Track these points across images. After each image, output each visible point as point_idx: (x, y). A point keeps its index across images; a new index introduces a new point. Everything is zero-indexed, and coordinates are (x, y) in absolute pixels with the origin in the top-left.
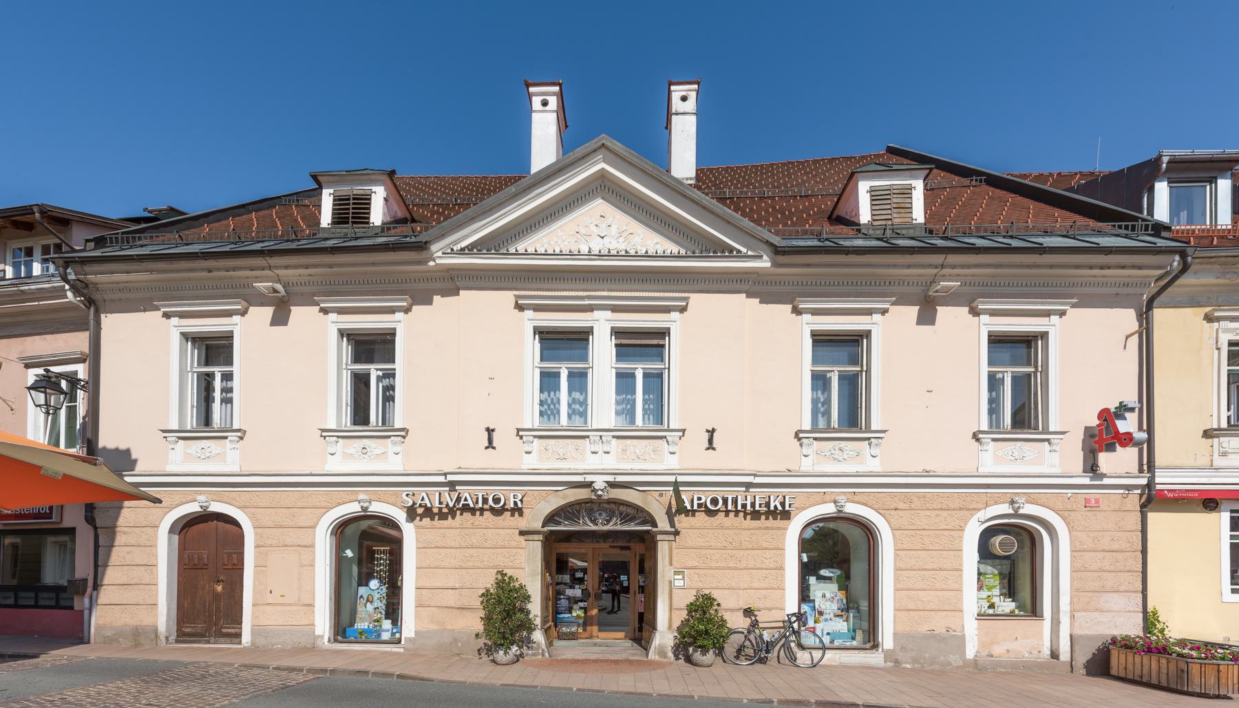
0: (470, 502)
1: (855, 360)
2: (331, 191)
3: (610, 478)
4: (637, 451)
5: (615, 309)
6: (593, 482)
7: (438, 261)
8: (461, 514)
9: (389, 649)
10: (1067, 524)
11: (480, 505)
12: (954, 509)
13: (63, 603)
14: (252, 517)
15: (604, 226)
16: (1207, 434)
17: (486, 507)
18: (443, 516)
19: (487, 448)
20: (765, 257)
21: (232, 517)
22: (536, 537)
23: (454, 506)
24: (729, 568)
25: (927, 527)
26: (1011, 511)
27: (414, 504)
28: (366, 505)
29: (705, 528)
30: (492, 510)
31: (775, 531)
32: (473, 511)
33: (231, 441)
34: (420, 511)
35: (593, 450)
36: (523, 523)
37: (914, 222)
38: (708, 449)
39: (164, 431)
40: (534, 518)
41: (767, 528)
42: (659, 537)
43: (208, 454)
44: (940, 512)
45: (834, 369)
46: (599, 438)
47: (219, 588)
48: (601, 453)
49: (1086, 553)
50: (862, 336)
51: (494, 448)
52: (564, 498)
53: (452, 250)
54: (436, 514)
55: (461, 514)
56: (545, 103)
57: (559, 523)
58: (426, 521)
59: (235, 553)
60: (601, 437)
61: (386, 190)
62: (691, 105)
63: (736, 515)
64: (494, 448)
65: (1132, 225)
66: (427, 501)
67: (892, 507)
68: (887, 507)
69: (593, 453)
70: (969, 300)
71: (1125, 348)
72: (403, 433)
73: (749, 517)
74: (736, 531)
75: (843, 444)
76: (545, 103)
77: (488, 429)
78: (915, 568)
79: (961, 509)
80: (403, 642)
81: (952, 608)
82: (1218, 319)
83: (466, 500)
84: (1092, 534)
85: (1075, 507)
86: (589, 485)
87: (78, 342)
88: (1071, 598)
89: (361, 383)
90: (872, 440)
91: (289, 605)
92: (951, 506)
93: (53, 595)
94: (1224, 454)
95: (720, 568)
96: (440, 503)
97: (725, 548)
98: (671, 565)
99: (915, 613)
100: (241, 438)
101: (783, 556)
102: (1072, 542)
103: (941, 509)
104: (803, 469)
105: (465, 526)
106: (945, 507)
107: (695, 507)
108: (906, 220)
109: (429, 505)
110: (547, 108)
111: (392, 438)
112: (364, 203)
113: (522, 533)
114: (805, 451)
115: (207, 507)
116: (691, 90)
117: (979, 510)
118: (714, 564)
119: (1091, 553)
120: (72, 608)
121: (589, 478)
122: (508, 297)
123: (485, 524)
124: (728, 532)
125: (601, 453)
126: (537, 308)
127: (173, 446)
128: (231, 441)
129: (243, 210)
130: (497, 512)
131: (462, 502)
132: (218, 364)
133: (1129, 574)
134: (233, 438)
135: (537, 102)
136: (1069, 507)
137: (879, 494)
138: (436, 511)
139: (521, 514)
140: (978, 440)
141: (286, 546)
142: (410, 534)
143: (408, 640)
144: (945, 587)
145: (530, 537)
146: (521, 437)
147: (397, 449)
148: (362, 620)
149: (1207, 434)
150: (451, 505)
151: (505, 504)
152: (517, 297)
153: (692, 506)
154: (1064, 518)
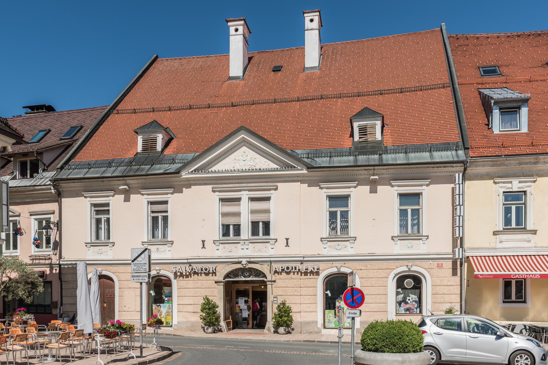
0: (196, 270)
2: (142, 136)
3: (248, 260)
4: (259, 248)
5: (249, 190)
6: (241, 261)
7: (184, 177)
8: (194, 275)
9: (168, 329)
10: (430, 274)
11: (200, 271)
12: (384, 269)
13: (47, 311)
14: (117, 277)
15: (245, 156)
16: (495, 233)
17: (202, 272)
18: (187, 276)
19: (202, 248)
20: (304, 169)
22: (221, 284)
23: (191, 272)
24: (295, 295)
25: (373, 277)
26: (407, 269)
27: (176, 271)
28: (158, 271)
29: (285, 279)
30: (205, 273)
31: (313, 279)
32: (197, 274)
33: (110, 247)
34: (179, 274)
35: (242, 248)
36: (216, 278)
37: (377, 139)
38: (286, 246)
39: (86, 243)
40: (220, 277)
41: (310, 278)
42: (268, 283)
43: (101, 252)
44: (378, 270)
45: (338, 210)
46: (244, 243)
47: (105, 305)
48: (245, 249)
49: (438, 287)
51: (205, 248)
52: (231, 268)
53: (188, 172)
54: (184, 275)
55: (194, 275)
56: (237, 30)
58: (181, 278)
59: (111, 291)
60: (245, 242)
61: (162, 135)
62: (315, 24)
63: (298, 274)
64: (205, 248)
65: (341, 212)
66: (181, 270)
67: (359, 268)
68: (357, 269)
69: (242, 249)
70: (388, 182)
72: (172, 243)
73: (303, 274)
74: (297, 280)
75: (339, 243)
76: (237, 30)
77: (202, 241)
78: (368, 294)
79: (387, 269)
80: (173, 326)
81: (383, 310)
82: (498, 183)
83: (195, 269)
84: (440, 279)
85: (433, 267)
86: (240, 263)
87: (53, 206)
88: (432, 306)
90: (350, 241)
91: (132, 311)
92: (383, 268)
93: (35, 308)
94: (501, 242)
95: (291, 295)
96: (186, 271)
97: (293, 287)
98: (272, 294)
99: (369, 313)
100: (113, 245)
101: (316, 290)
102: (432, 282)
103: (379, 269)
104: (324, 254)
105: (195, 279)
106: (380, 268)
107: (281, 271)
108: (373, 139)
109: (182, 272)
110: (238, 33)
111: (168, 245)
112: (155, 141)
113: (216, 282)
115: (101, 273)
116: (316, 16)
117: (394, 269)
118: (289, 294)
119: (439, 287)
120: (52, 313)
121: (240, 260)
122: (209, 187)
123: (202, 279)
124: (294, 280)
125: (245, 249)
126: (220, 191)
127: (89, 249)
128: (110, 247)
129: (98, 126)
130: (207, 274)
131: (193, 270)
133: (455, 295)
134: (110, 246)
135: (232, 30)
136: (430, 267)
137: (354, 263)
138: (184, 274)
139: (216, 275)
140: (393, 240)
141: (130, 288)
142: (174, 282)
143: (175, 325)
144: (380, 302)
145: (219, 284)
146: (215, 243)
147: (169, 249)
148: (457, 156)
149: (495, 233)
150: (189, 272)
151: (209, 271)
152: (213, 188)
154: (428, 272)
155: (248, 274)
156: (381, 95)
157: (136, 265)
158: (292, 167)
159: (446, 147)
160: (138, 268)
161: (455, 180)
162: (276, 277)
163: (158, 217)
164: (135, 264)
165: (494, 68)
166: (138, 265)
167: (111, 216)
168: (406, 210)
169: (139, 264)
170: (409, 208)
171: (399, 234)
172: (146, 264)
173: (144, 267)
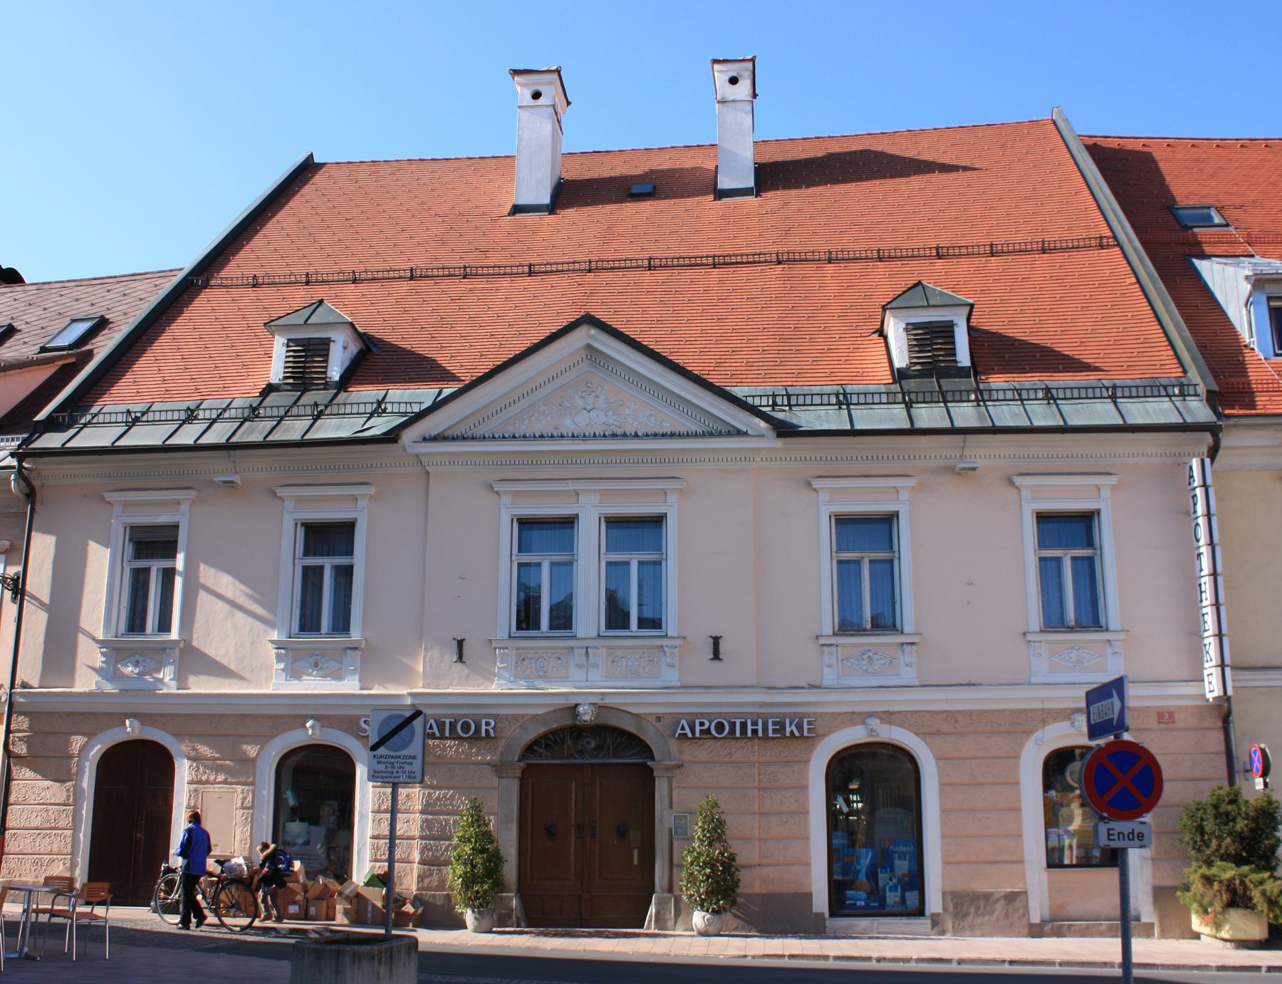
1: (1090, 543)
21: (101, 758)
50: (892, 515)
57: (540, 756)
71: (516, 72)
89: (311, 577)
98: (671, 807)
114: (827, 660)
132: (330, 553)
153: (693, 732)
155: (593, 744)
156: (940, 259)
157: (382, 760)
158: (739, 433)
159: (1156, 389)
160: (390, 769)
161: (1191, 477)
162: (690, 753)
163: (321, 568)
164: (381, 757)
165: (1206, 211)
166: (390, 760)
167: (359, 560)
168: (1058, 560)
169: (392, 757)
170: (632, 556)
171: (1042, 625)
172: (414, 757)
173: (407, 768)
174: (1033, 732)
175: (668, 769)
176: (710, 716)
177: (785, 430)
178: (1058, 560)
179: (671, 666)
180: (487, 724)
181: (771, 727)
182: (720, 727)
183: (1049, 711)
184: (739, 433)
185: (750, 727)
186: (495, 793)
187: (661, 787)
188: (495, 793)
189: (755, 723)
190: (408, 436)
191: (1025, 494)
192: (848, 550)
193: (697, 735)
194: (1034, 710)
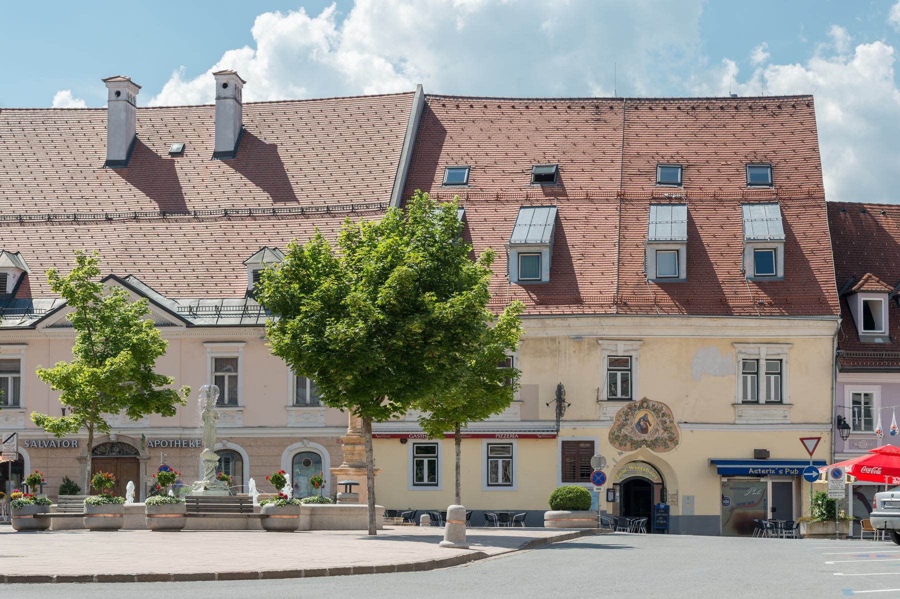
158: (175, 325)
167: (22, 375)
168: (223, 377)
174: (288, 446)
175: (145, 459)
176: (161, 439)
177: (189, 325)
178: (223, 377)
179: (21, 420)
180: (74, 442)
181: (184, 443)
182: (164, 443)
183: (294, 438)
184: (175, 325)
185: (176, 443)
186: (78, 469)
187: (142, 466)
188: (78, 469)
189: (177, 442)
190: (39, 326)
191: (209, 350)
192: (219, 371)
193: (156, 446)
194: (288, 438)
